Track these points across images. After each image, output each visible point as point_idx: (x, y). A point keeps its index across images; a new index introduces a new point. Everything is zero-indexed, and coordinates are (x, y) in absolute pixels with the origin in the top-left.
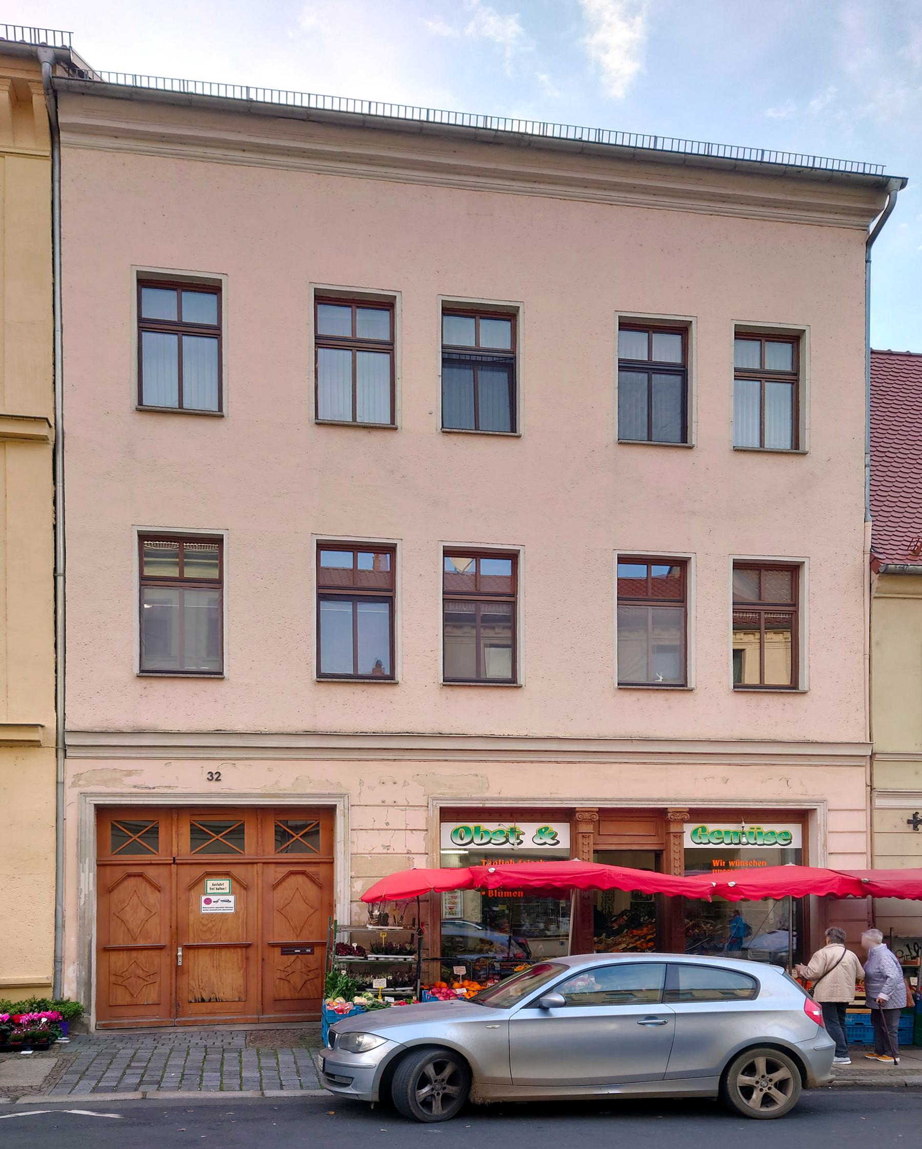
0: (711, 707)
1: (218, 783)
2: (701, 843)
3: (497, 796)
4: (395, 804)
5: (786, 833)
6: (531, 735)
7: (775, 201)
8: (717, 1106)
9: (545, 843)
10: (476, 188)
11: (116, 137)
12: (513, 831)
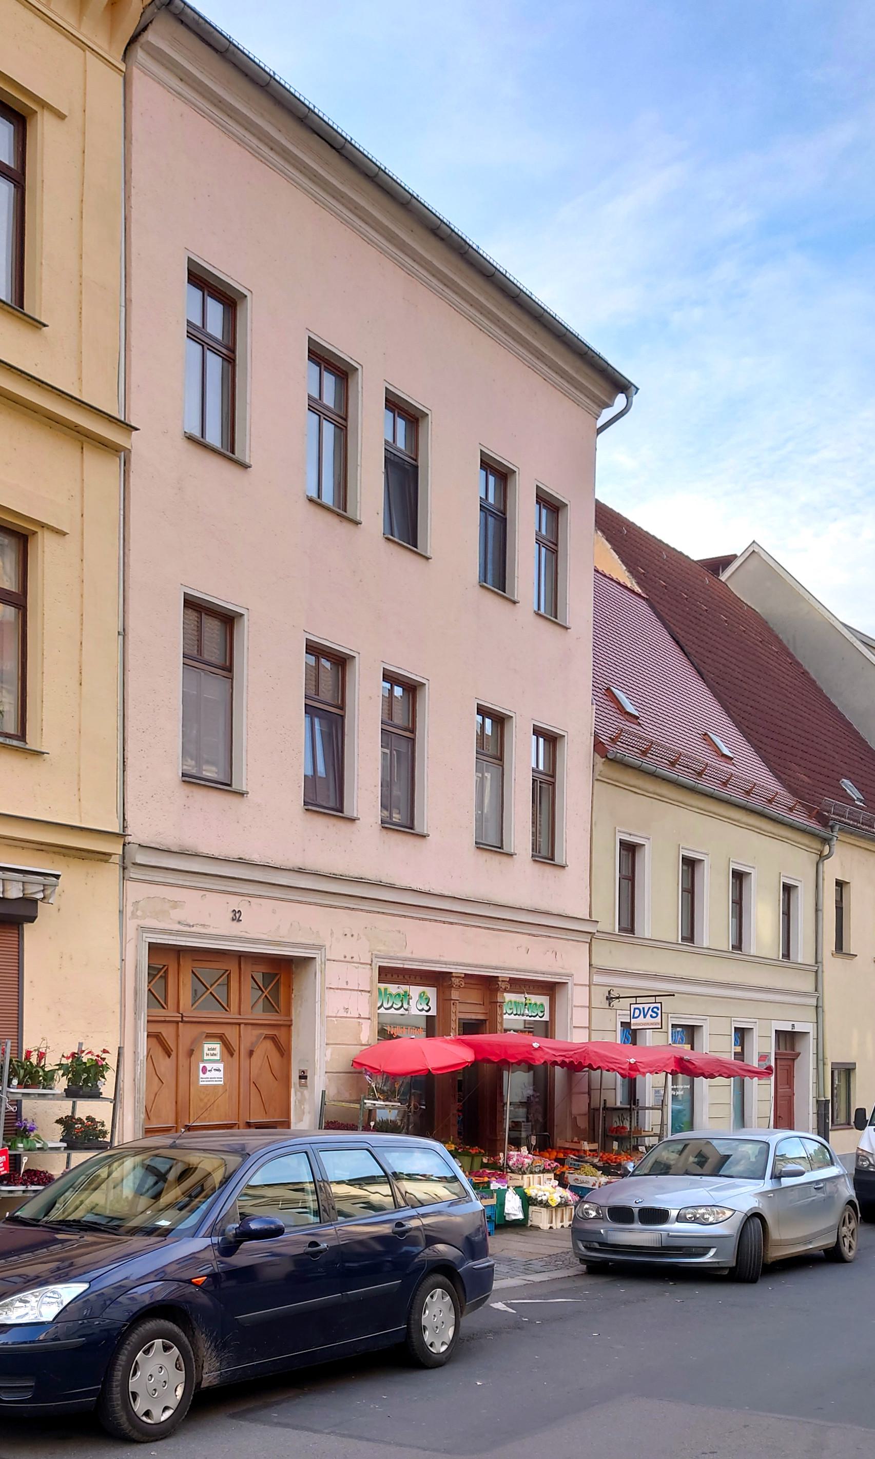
1: (239, 924)
3: (410, 956)
6: (432, 891)
7: (565, 372)
9: (423, 1010)
11: (181, 80)
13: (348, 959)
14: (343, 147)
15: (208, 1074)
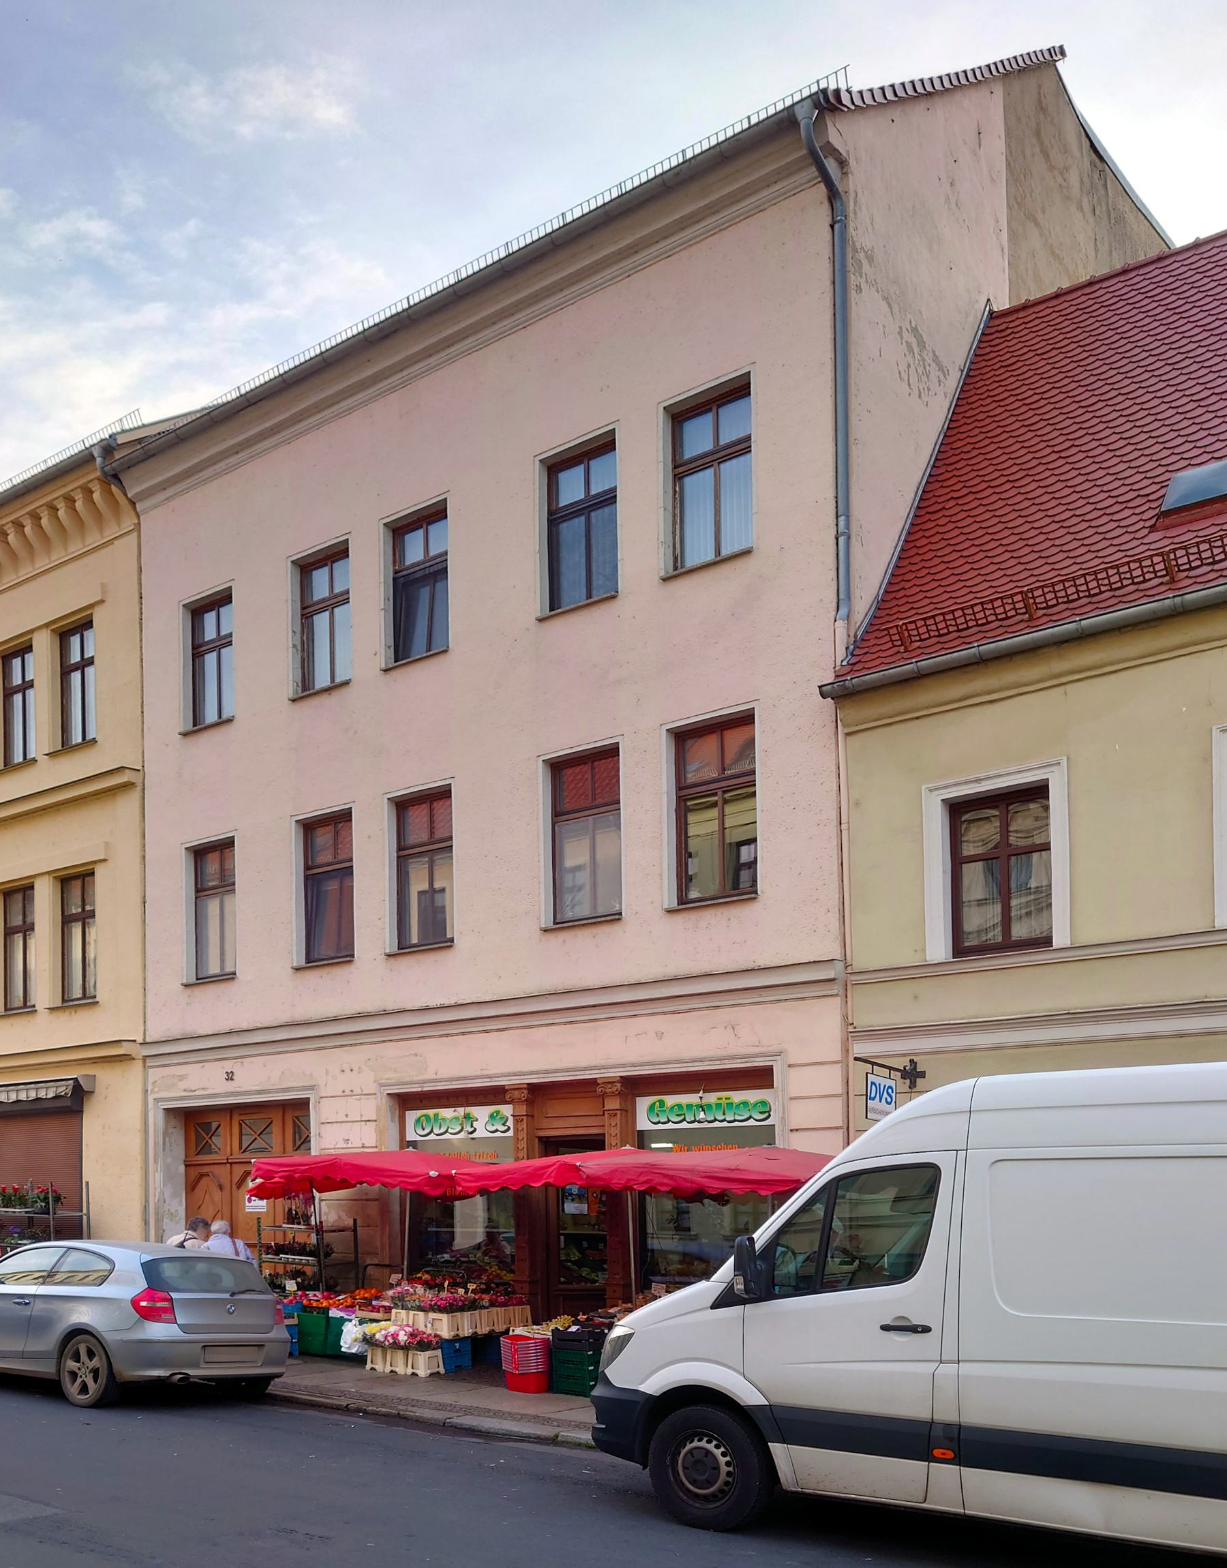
0: (652, 938)
2: (735, 1121)
3: (434, 1077)
4: (352, 1094)
5: (764, 1103)
8: (47, 1388)
9: (497, 1131)
10: (404, 384)
12: (467, 1117)
13: (348, 1092)
14: (248, 400)
15: (253, 1203)
